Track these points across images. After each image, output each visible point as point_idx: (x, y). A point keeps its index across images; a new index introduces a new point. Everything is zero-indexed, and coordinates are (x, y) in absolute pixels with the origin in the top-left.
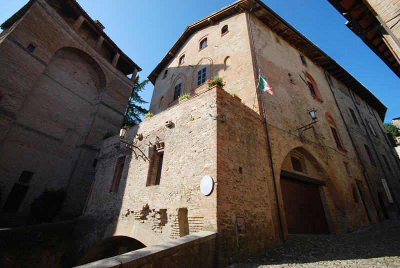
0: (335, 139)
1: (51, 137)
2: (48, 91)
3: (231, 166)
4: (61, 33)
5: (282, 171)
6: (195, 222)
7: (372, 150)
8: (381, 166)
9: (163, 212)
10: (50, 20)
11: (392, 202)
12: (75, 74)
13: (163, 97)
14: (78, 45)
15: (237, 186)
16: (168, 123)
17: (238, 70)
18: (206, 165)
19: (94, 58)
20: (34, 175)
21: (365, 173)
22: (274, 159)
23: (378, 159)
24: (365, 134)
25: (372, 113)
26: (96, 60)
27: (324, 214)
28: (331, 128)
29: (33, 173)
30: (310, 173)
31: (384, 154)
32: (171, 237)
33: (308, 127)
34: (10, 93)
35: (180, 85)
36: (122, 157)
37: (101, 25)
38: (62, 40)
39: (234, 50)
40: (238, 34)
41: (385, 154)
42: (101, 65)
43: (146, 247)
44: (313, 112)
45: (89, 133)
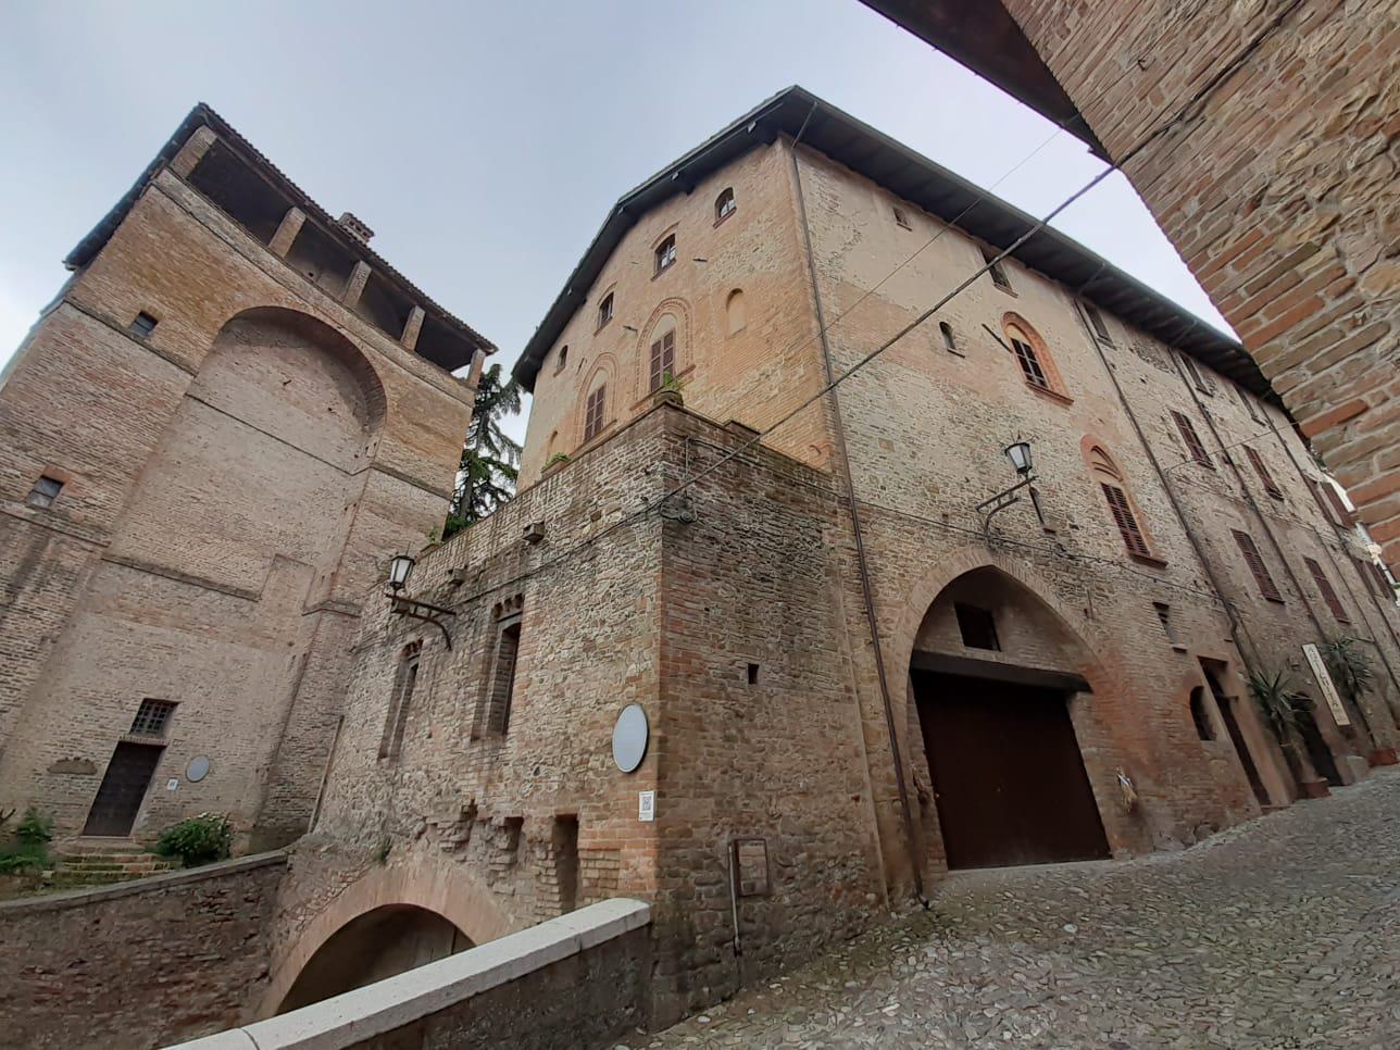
0: (1121, 524)
1: (224, 590)
2: (206, 446)
3: (716, 661)
4: (236, 268)
5: (916, 655)
6: (598, 864)
7: (1262, 545)
8: (1302, 597)
9: (515, 825)
10: (196, 233)
11: (1347, 722)
12: (288, 387)
13: (556, 433)
14: (287, 301)
15: (740, 731)
16: (532, 530)
17: (764, 333)
18: (633, 669)
19: (343, 332)
20: (179, 709)
21: (1239, 630)
22: (885, 621)
23: (1289, 572)
24: (1238, 492)
25: (1261, 417)
26: (351, 338)
27: (1090, 788)
28: (1105, 487)
29: (174, 705)
30: (1019, 651)
31: (1312, 556)
32: (538, 911)
33: (1004, 501)
34: (87, 468)
35: (601, 392)
36: (413, 644)
37: (360, 227)
38: (239, 288)
39: (752, 270)
40: (764, 216)
41: (1318, 555)
42: (366, 351)
43: (1234, 531)
44: (1018, 448)
45: (340, 564)
